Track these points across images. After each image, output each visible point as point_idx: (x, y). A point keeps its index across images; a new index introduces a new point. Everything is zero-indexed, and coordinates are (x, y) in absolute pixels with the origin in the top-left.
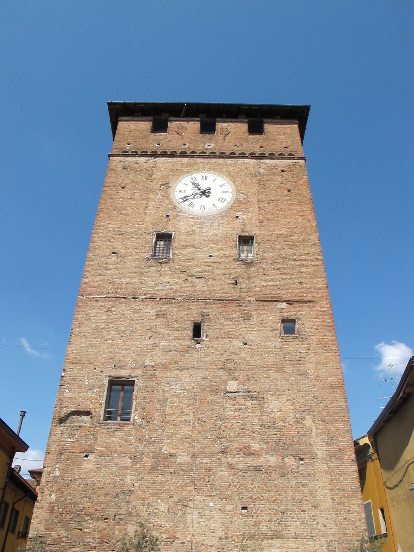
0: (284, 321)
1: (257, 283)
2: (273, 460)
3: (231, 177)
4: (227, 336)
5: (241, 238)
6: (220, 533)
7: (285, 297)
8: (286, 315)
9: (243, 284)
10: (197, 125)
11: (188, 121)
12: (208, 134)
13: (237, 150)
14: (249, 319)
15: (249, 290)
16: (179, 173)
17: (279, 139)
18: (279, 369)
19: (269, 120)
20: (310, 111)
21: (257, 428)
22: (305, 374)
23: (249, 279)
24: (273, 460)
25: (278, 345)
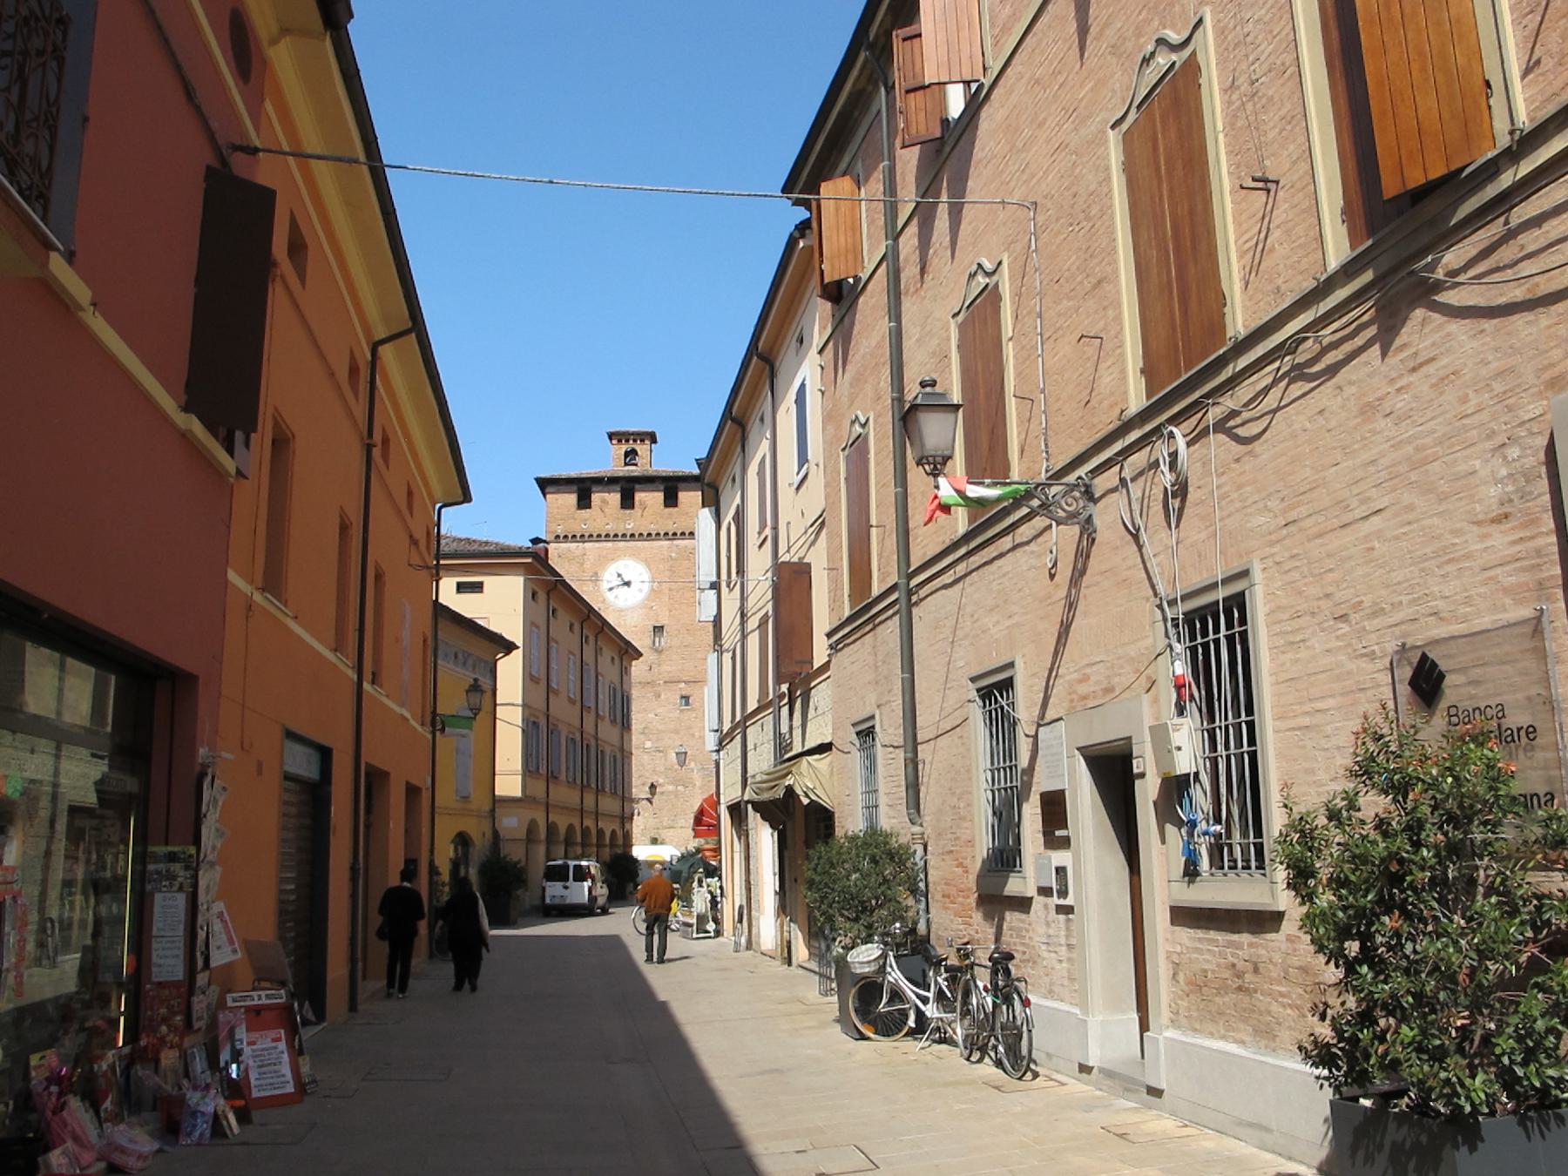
0: (682, 697)
1: (665, 668)
2: (671, 788)
3: (647, 562)
4: (645, 710)
5: (655, 627)
6: (642, 827)
7: (684, 679)
8: (684, 693)
9: (655, 669)
10: (618, 496)
11: (609, 492)
12: (49, 648)
13: (653, 529)
14: (659, 696)
15: (660, 674)
16: (605, 560)
17: (42, 910)
18: (676, 732)
19: (600, 488)
20: (1154, 1086)
21: (662, 769)
22: (693, 735)
23: (659, 665)
24: (671, 788)
25: (677, 715)
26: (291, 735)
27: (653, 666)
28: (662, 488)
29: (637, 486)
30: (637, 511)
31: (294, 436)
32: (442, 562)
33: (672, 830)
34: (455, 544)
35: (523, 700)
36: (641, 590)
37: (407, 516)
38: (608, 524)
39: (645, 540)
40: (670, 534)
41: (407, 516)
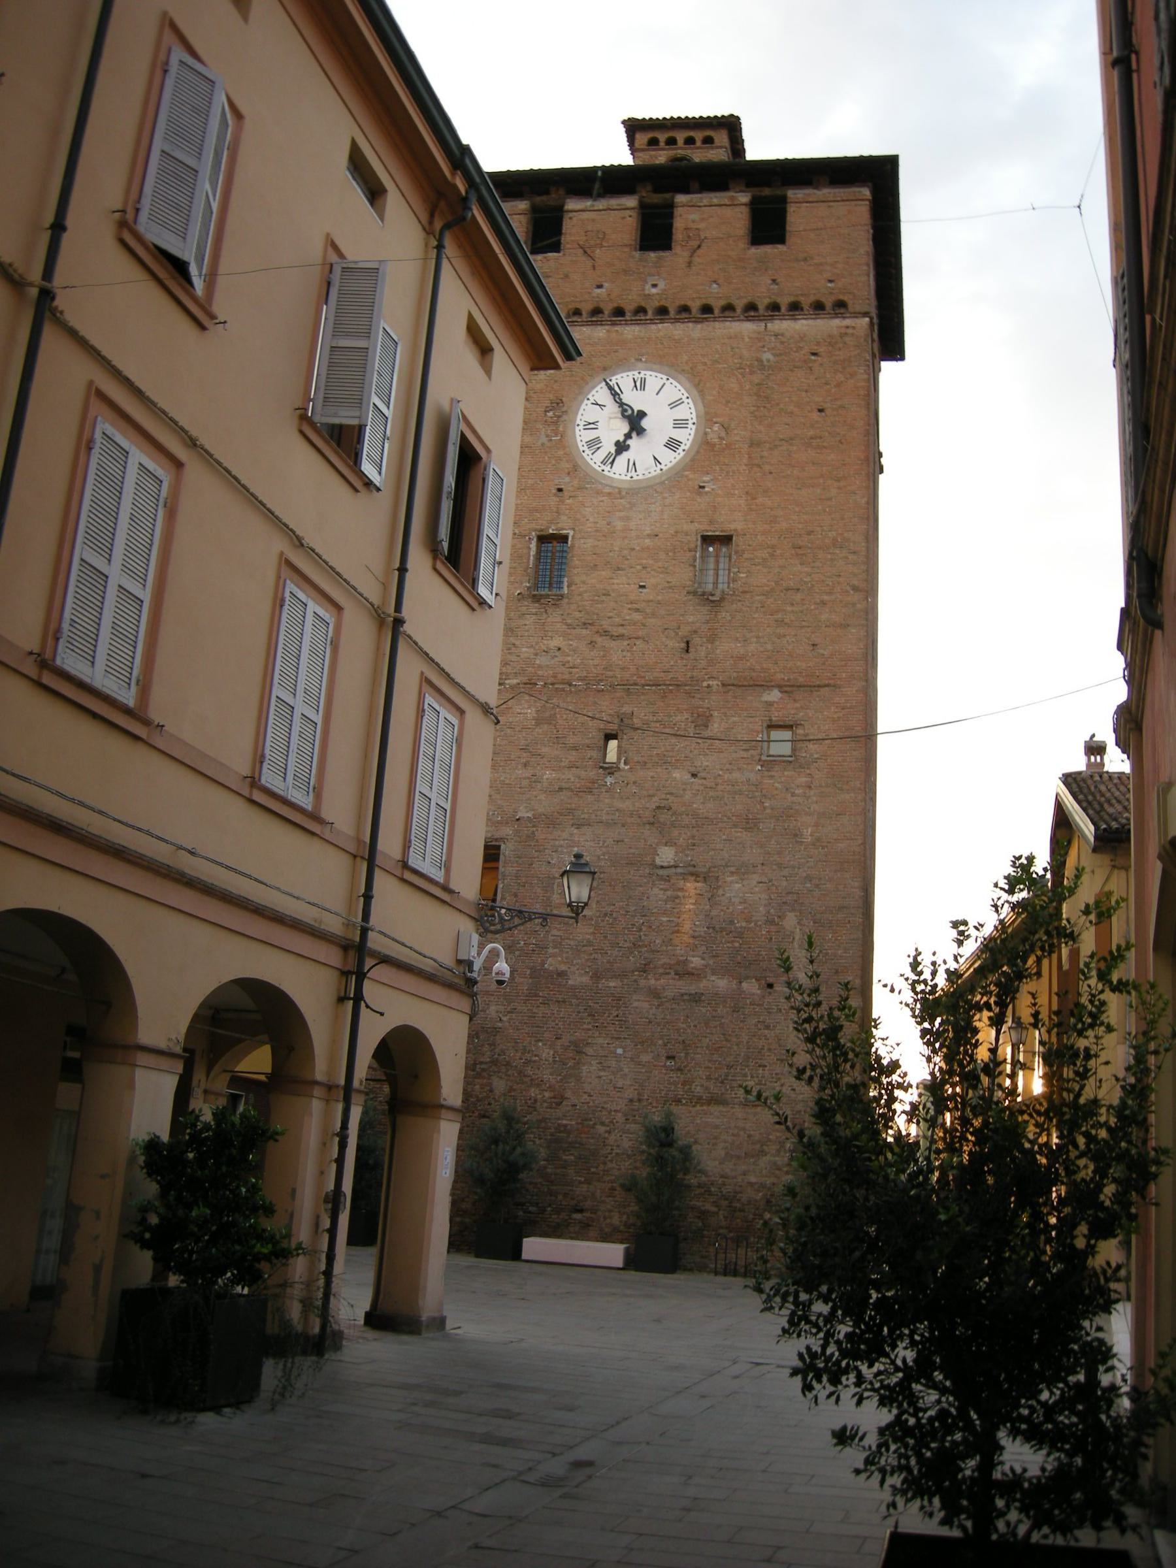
1: (726, 647)
2: (722, 984)
9: (700, 650)
13: (716, 295)
18: (750, 823)
22: (796, 835)
23: (712, 639)
24: (722, 984)
26: (114, 212)
27: (696, 640)
28: (744, 198)
29: (792, 194)
30: (678, 255)
31: (488, 450)
32: (352, 996)
33: (714, 1109)
34: (805, 921)
35: (467, 1095)
36: (672, 444)
37: (198, 66)
38: (600, 287)
39: (697, 321)
40: (761, 307)
41: (198, 66)
